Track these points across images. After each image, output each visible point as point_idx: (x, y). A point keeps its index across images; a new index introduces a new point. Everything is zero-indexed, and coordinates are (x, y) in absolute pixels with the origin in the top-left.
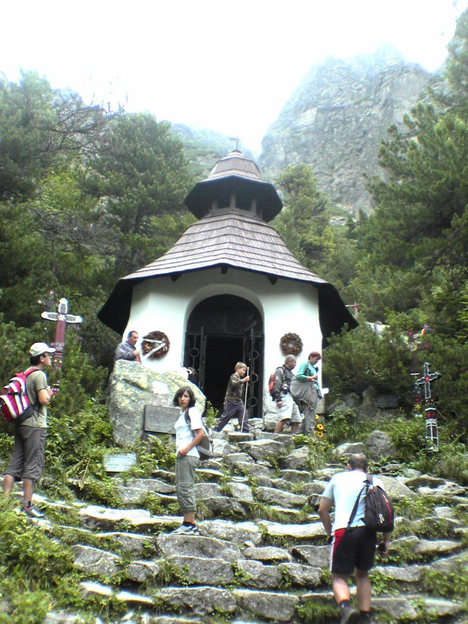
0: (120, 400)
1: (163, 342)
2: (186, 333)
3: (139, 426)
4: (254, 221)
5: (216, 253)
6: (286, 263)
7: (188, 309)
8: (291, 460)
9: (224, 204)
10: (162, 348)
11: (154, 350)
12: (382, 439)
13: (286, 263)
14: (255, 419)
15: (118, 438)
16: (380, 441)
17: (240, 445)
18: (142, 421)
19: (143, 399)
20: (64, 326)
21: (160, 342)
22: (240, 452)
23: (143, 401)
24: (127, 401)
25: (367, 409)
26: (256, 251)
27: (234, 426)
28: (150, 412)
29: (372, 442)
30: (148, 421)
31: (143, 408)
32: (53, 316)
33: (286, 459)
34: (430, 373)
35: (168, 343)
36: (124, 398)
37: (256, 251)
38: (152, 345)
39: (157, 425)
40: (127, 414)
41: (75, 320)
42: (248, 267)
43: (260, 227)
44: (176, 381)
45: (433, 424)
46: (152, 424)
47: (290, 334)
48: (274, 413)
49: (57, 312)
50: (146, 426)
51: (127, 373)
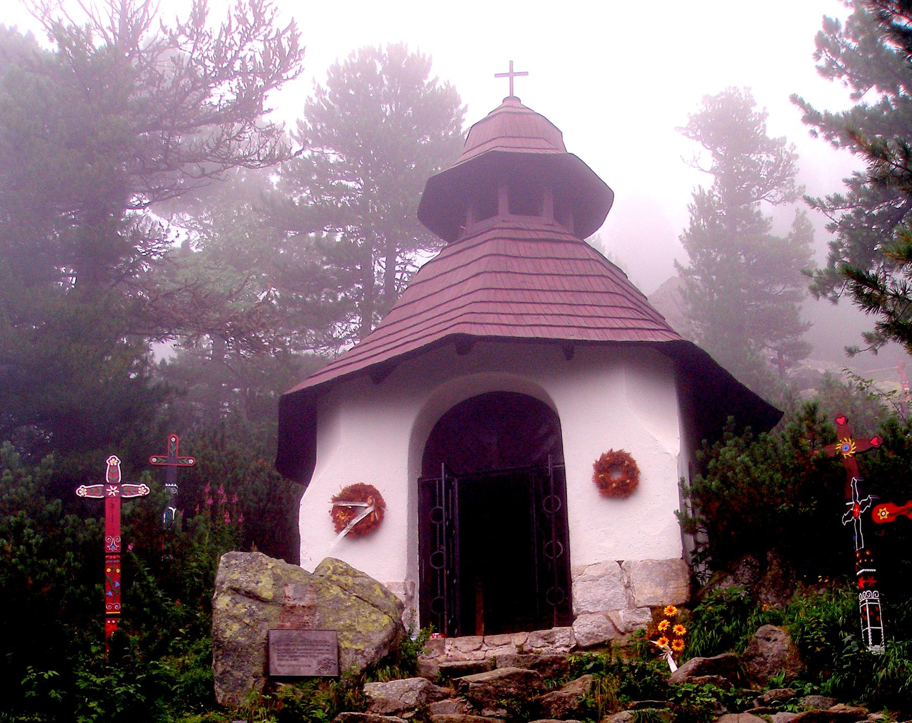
0: (223, 626)
1: (371, 505)
2: (419, 480)
3: (258, 669)
4: (542, 235)
5: (523, 309)
6: (599, 312)
7: (416, 433)
8: (550, 703)
9: (488, 211)
10: (369, 515)
11: (355, 521)
12: (775, 640)
13: (599, 312)
14: (555, 629)
15: (221, 696)
16: (769, 645)
17: (456, 684)
18: (263, 659)
19: (266, 620)
20: (118, 505)
21: (365, 505)
22: (455, 697)
23: (266, 624)
24: (236, 627)
25: (774, 582)
26: (542, 297)
27: (517, 646)
28: (278, 642)
29: (756, 649)
30: (274, 656)
31: (265, 636)
32: (97, 491)
33: (543, 699)
34: (860, 500)
35: (380, 506)
36: (230, 622)
37: (542, 297)
38: (353, 512)
39: (294, 663)
40: (235, 650)
41: (137, 492)
42: (531, 335)
43: (555, 246)
44: (334, 578)
45: (869, 601)
46: (283, 663)
47: (611, 453)
48: (591, 613)
49: (104, 482)
50: (272, 667)
51: (235, 576)
